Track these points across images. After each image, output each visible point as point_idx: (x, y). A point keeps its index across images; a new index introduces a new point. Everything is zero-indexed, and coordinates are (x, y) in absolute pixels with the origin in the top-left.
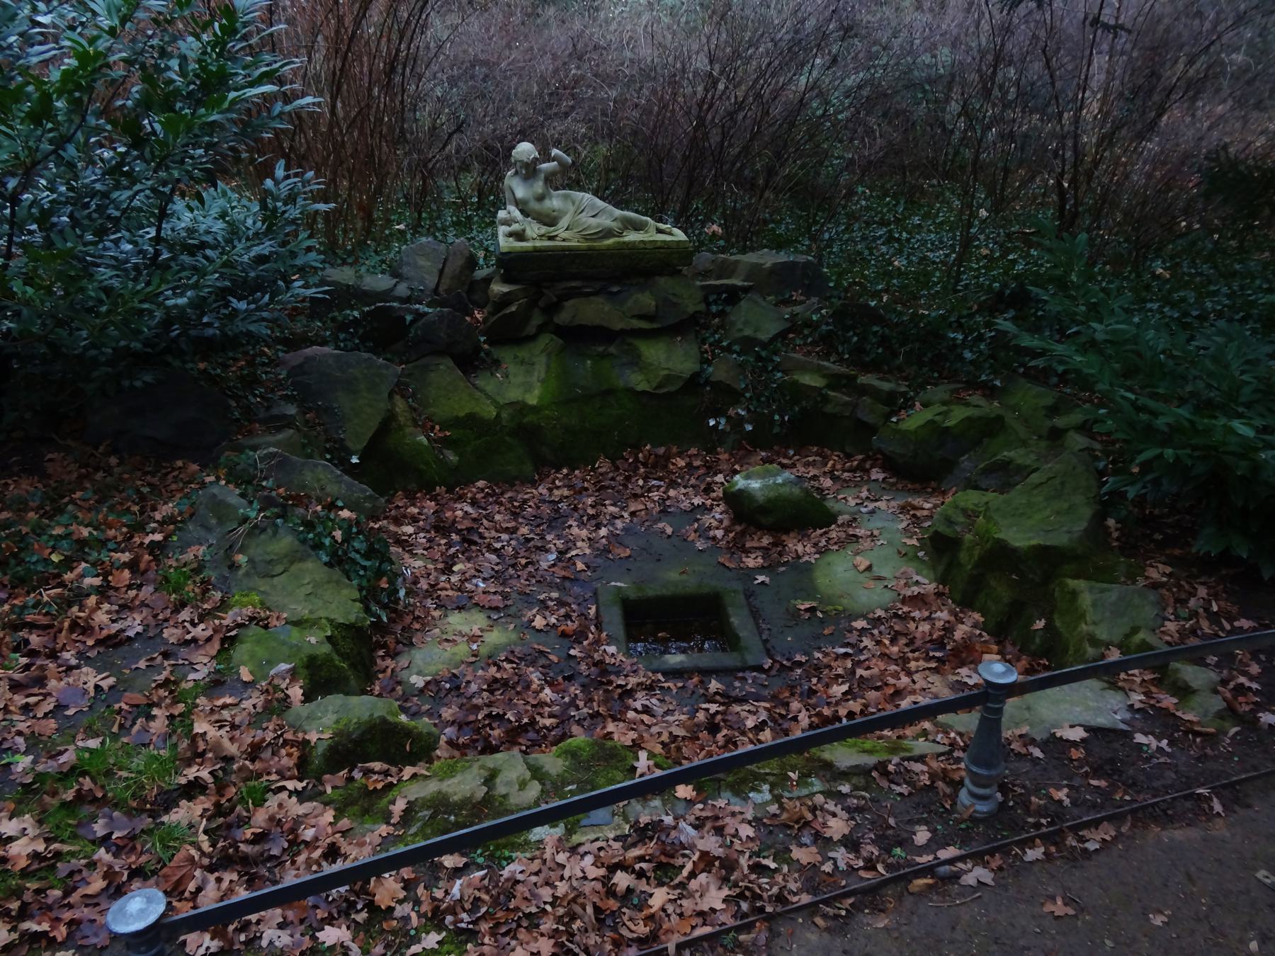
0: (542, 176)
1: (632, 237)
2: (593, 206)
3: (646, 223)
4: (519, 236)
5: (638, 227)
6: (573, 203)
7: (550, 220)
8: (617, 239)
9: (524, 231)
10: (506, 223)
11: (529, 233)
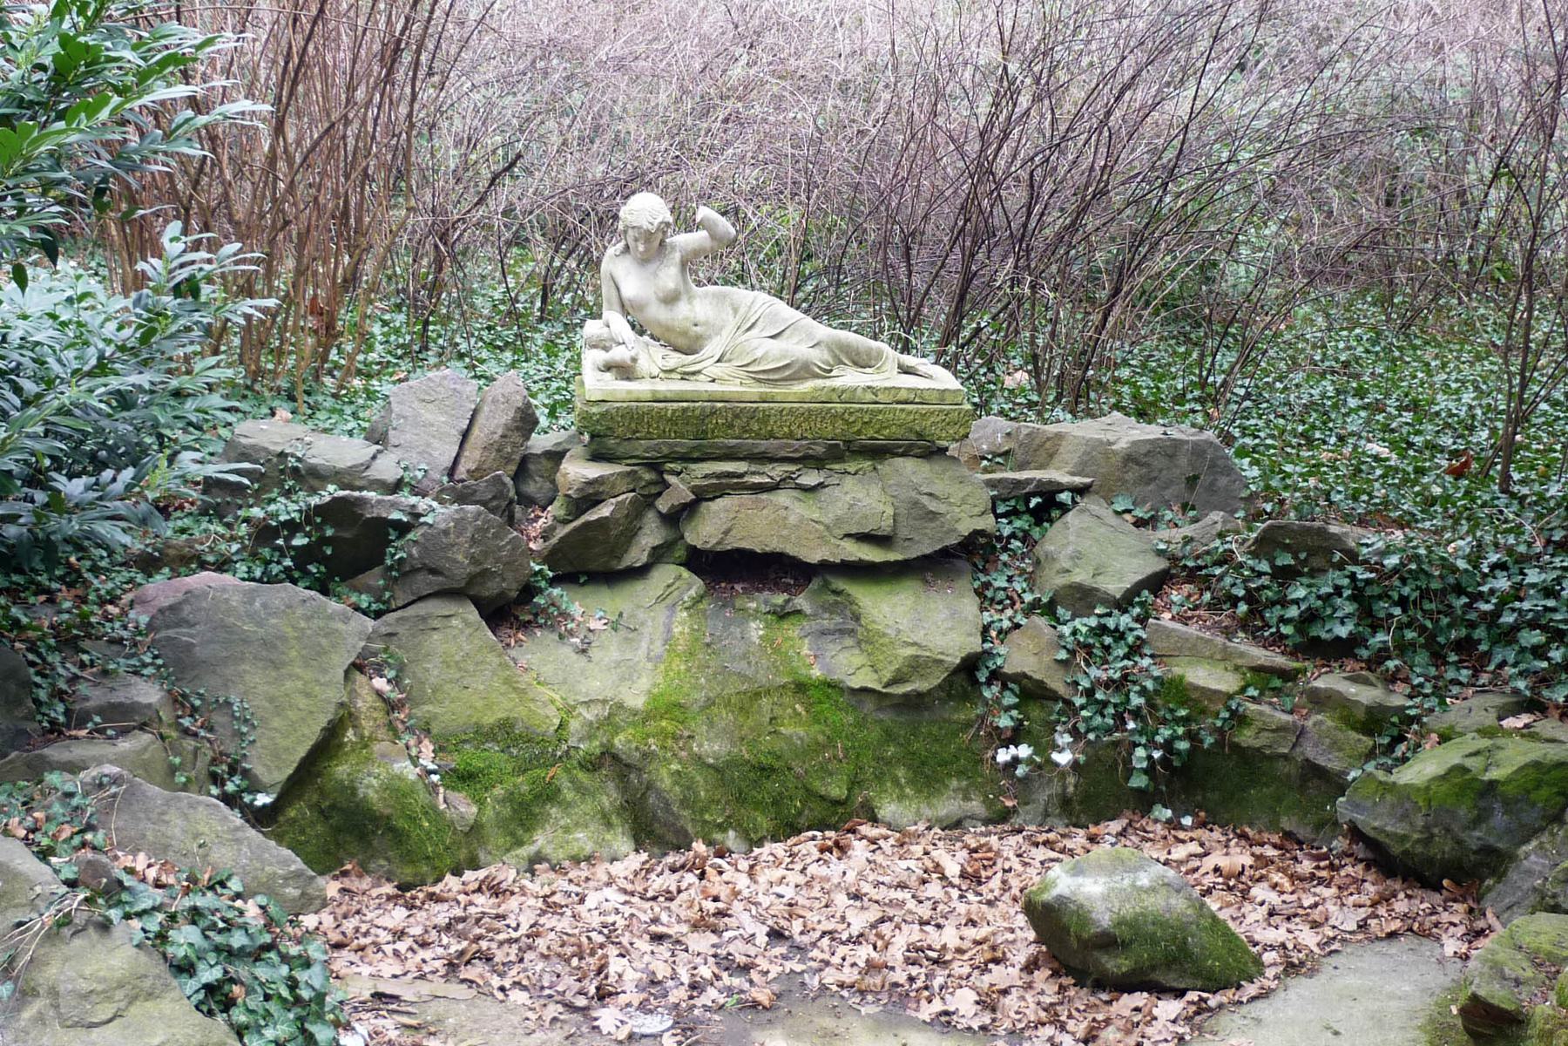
0: (677, 256)
1: (850, 378)
3: (880, 355)
4: (624, 371)
5: (861, 361)
6: (736, 311)
7: (687, 344)
8: (819, 383)
9: (634, 360)
10: (601, 345)
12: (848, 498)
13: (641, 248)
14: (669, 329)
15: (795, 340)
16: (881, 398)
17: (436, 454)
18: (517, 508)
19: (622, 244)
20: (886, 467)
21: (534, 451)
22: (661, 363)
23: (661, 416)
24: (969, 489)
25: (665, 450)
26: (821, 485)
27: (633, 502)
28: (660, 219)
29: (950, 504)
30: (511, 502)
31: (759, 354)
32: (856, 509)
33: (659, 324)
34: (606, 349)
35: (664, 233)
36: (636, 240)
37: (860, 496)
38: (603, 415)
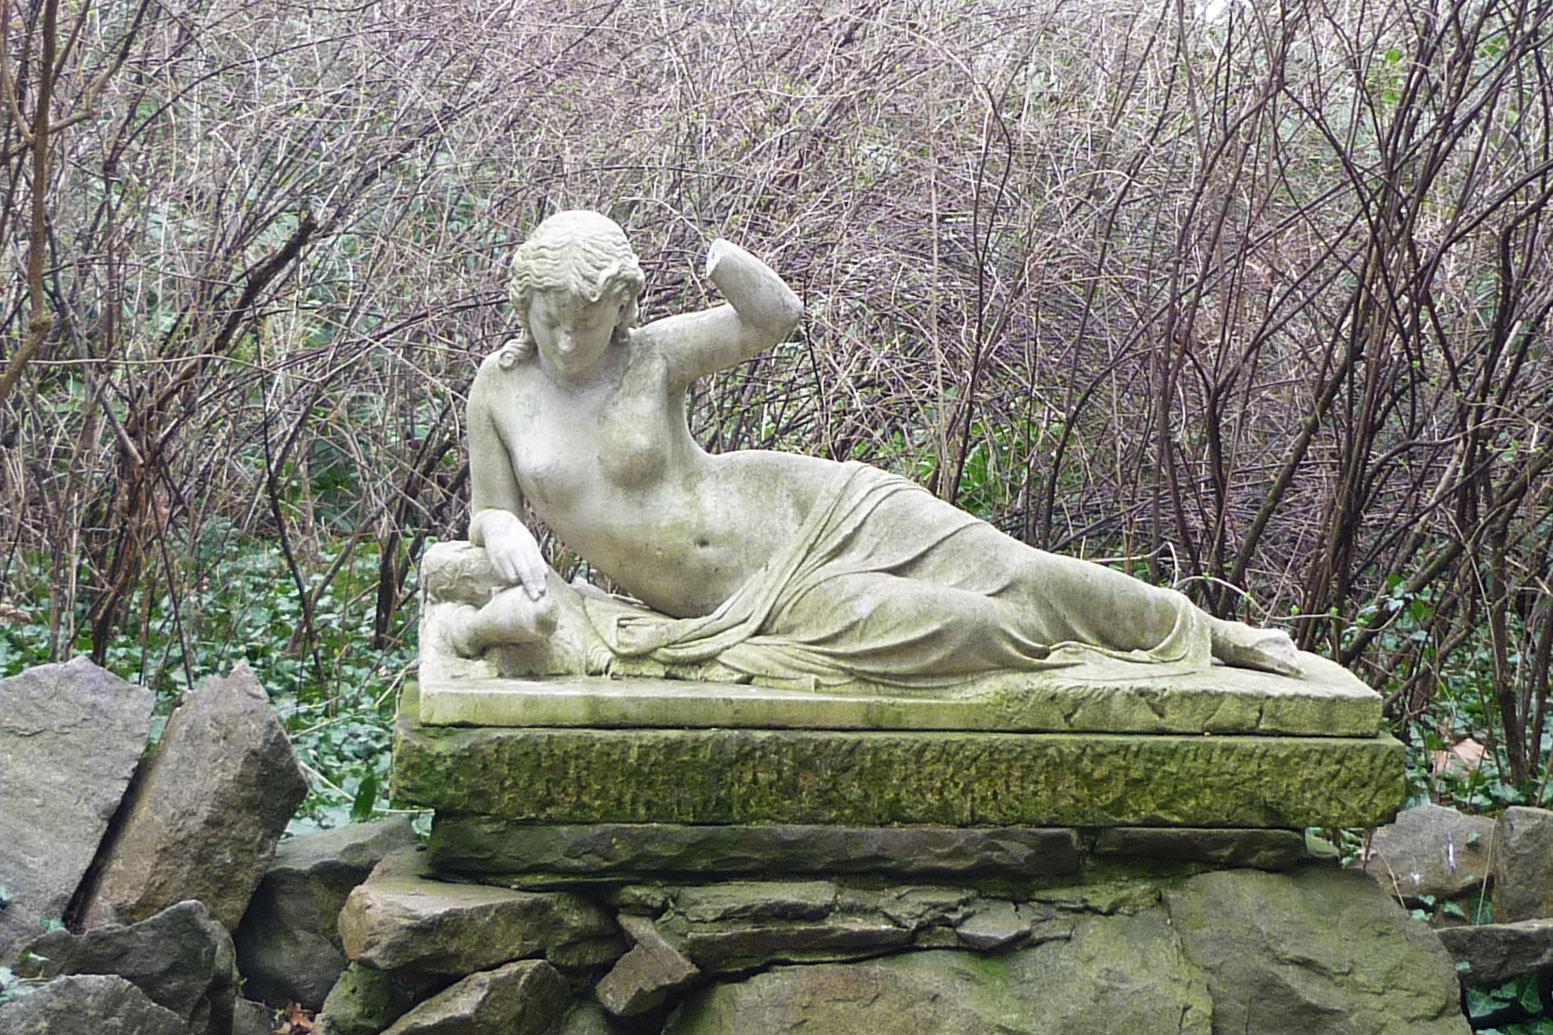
0: (657, 369)
1: (1091, 671)
2: (901, 524)
3: (1167, 618)
4: (519, 652)
5: (1119, 633)
6: (803, 508)
7: (678, 587)
8: (1017, 681)
9: (546, 625)
10: (465, 590)
11: (572, 639)
12: (1093, 972)
13: (565, 344)
14: (635, 553)
15: (955, 577)
16: (1173, 718)
17: (35, 863)
18: (241, 1006)
19: (521, 339)
20: (1188, 897)
21: (294, 864)
22: (613, 636)
23: (610, 763)
24: (1402, 951)
25: (623, 852)
26: (1023, 942)
27: (536, 983)
28: (612, 270)
29: (1357, 988)
30: (221, 984)
31: (863, 608)
32: (1115, 1000)
33: (612, 541)
34: (476, 601)
35: (624, 309)
36: (553, 324)
37: (1126, 966)
38: (462, 760)
